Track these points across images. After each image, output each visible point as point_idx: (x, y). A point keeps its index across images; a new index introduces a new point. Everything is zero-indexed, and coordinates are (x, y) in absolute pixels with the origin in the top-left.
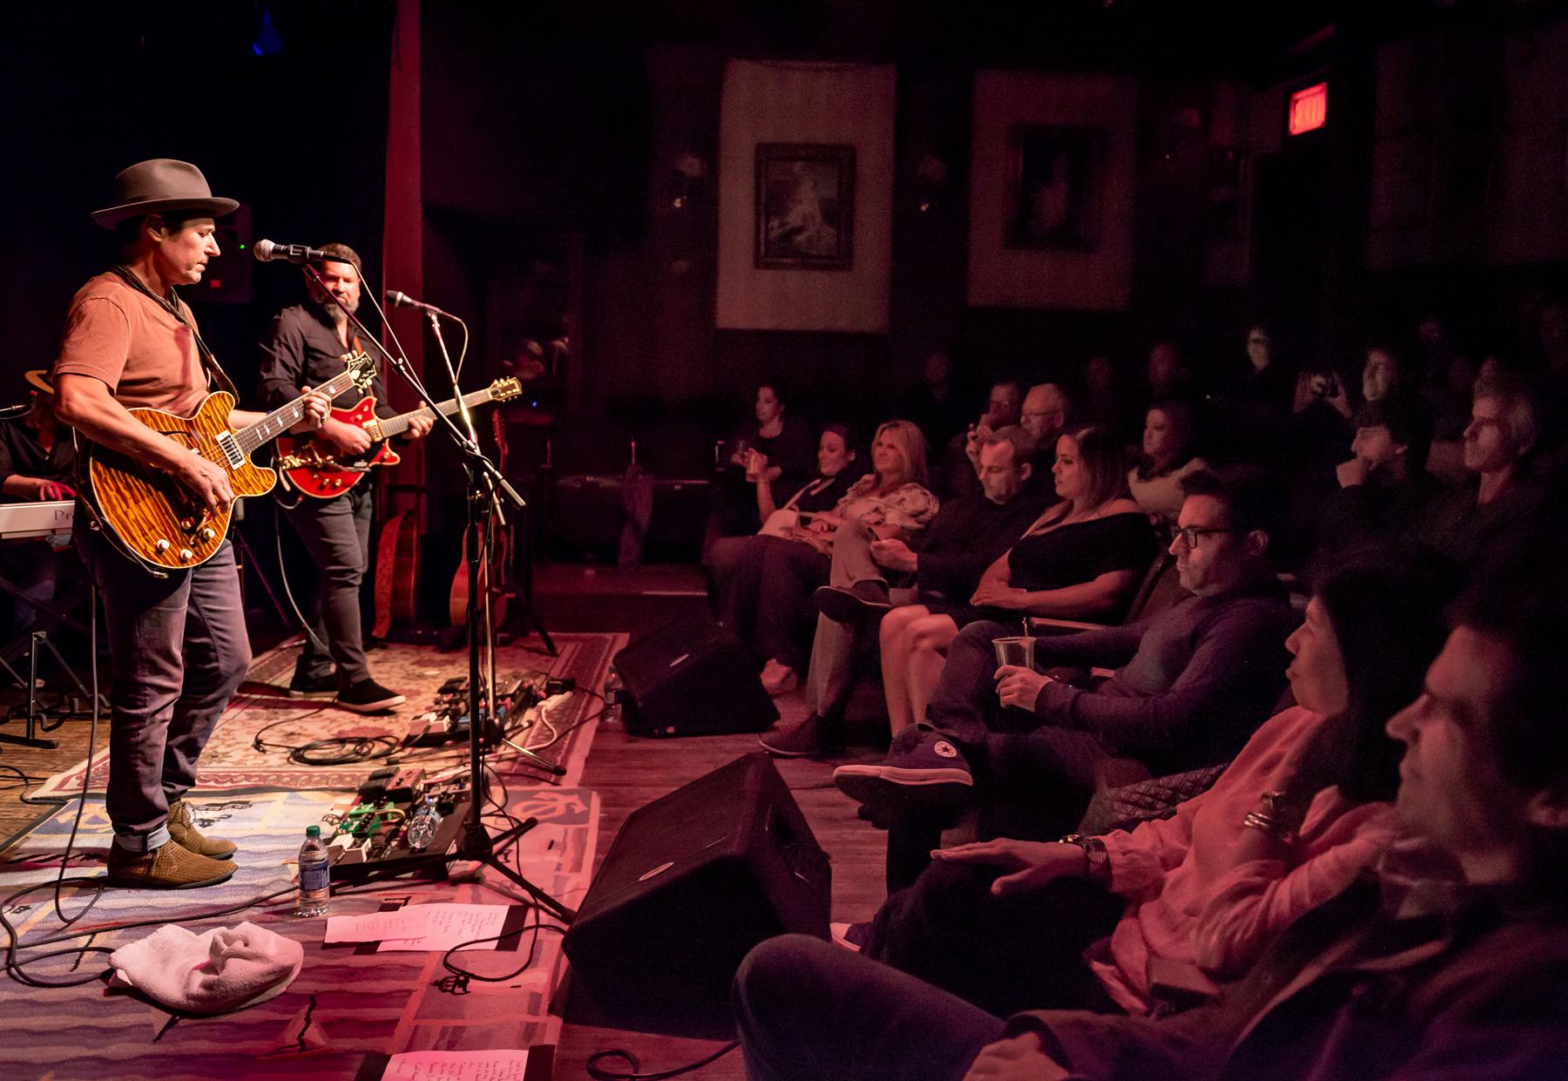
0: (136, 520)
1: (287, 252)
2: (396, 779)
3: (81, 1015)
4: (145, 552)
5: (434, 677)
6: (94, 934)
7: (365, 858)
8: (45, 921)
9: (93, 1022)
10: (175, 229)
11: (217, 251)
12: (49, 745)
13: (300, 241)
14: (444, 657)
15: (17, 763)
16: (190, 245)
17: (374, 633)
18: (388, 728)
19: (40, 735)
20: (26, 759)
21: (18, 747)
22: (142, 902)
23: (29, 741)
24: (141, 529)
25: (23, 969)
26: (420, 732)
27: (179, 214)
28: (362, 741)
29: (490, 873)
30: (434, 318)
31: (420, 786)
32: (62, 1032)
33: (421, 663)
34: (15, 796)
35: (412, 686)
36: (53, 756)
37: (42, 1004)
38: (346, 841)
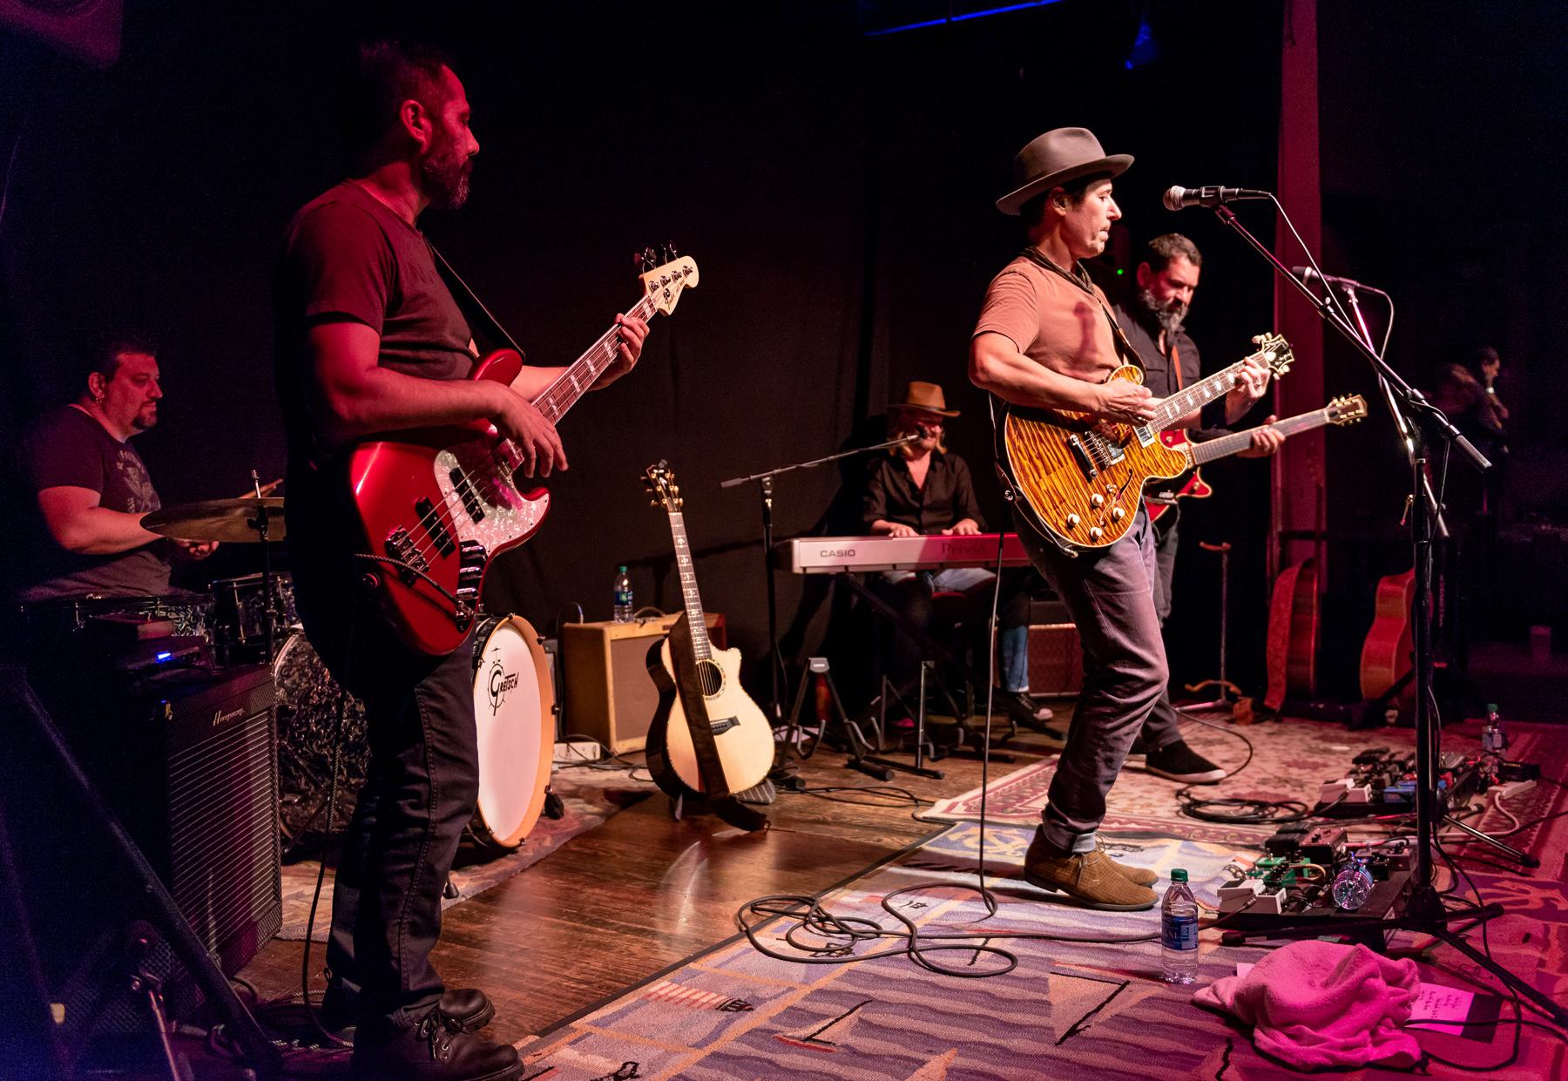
0: (1048, 492)
1: (1198, 195)
2: (1312, 835)
3: (981, 1005)
4: (1056, 525)
5: (1344, 753)
6: (988, 938)
7: (1280, 911)
8: (941, 918)
9: (993, 1014)
10: (1077, 199)
11: (1119, 213)
12: (936, 775)
13: (1212, 181)
14: (1355, 735)
15: (908, 788)
16: (1094, 212)
17: (1267, 703)
18: (1292, 796)
19: (927, 765)
20: (919, 786)
21: (907, 775)
22: (1034, 918)
23: (917, 771)
24: (1052, 500)
25: (924, 955)
26: (1334, 800)
27: (1078, 182)
28: (1263, 805)
29: (1447, 954)
30: (1351, 292)
31: (1342, 848)
32: (964, 1016)
33: (1324, 738)
34: (907, 813)
35: (1317, 759)
36: (939, 785)
37: (950, 990)
38: (1258, 886)
